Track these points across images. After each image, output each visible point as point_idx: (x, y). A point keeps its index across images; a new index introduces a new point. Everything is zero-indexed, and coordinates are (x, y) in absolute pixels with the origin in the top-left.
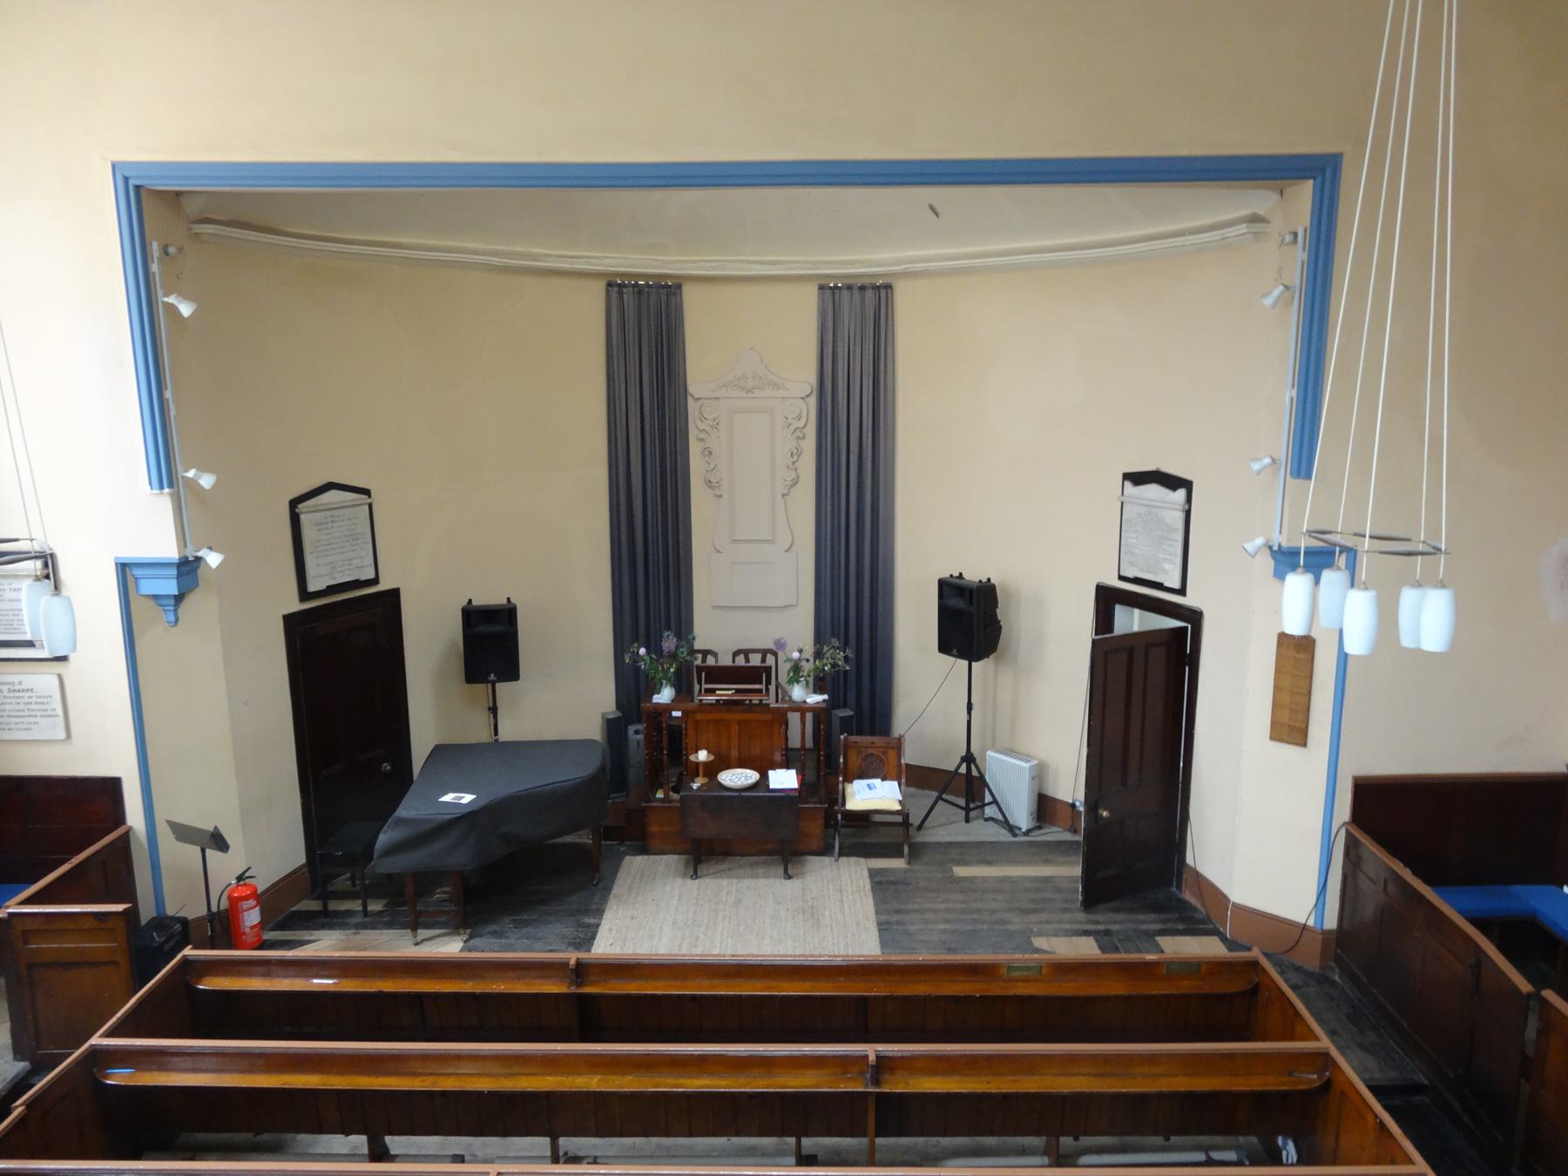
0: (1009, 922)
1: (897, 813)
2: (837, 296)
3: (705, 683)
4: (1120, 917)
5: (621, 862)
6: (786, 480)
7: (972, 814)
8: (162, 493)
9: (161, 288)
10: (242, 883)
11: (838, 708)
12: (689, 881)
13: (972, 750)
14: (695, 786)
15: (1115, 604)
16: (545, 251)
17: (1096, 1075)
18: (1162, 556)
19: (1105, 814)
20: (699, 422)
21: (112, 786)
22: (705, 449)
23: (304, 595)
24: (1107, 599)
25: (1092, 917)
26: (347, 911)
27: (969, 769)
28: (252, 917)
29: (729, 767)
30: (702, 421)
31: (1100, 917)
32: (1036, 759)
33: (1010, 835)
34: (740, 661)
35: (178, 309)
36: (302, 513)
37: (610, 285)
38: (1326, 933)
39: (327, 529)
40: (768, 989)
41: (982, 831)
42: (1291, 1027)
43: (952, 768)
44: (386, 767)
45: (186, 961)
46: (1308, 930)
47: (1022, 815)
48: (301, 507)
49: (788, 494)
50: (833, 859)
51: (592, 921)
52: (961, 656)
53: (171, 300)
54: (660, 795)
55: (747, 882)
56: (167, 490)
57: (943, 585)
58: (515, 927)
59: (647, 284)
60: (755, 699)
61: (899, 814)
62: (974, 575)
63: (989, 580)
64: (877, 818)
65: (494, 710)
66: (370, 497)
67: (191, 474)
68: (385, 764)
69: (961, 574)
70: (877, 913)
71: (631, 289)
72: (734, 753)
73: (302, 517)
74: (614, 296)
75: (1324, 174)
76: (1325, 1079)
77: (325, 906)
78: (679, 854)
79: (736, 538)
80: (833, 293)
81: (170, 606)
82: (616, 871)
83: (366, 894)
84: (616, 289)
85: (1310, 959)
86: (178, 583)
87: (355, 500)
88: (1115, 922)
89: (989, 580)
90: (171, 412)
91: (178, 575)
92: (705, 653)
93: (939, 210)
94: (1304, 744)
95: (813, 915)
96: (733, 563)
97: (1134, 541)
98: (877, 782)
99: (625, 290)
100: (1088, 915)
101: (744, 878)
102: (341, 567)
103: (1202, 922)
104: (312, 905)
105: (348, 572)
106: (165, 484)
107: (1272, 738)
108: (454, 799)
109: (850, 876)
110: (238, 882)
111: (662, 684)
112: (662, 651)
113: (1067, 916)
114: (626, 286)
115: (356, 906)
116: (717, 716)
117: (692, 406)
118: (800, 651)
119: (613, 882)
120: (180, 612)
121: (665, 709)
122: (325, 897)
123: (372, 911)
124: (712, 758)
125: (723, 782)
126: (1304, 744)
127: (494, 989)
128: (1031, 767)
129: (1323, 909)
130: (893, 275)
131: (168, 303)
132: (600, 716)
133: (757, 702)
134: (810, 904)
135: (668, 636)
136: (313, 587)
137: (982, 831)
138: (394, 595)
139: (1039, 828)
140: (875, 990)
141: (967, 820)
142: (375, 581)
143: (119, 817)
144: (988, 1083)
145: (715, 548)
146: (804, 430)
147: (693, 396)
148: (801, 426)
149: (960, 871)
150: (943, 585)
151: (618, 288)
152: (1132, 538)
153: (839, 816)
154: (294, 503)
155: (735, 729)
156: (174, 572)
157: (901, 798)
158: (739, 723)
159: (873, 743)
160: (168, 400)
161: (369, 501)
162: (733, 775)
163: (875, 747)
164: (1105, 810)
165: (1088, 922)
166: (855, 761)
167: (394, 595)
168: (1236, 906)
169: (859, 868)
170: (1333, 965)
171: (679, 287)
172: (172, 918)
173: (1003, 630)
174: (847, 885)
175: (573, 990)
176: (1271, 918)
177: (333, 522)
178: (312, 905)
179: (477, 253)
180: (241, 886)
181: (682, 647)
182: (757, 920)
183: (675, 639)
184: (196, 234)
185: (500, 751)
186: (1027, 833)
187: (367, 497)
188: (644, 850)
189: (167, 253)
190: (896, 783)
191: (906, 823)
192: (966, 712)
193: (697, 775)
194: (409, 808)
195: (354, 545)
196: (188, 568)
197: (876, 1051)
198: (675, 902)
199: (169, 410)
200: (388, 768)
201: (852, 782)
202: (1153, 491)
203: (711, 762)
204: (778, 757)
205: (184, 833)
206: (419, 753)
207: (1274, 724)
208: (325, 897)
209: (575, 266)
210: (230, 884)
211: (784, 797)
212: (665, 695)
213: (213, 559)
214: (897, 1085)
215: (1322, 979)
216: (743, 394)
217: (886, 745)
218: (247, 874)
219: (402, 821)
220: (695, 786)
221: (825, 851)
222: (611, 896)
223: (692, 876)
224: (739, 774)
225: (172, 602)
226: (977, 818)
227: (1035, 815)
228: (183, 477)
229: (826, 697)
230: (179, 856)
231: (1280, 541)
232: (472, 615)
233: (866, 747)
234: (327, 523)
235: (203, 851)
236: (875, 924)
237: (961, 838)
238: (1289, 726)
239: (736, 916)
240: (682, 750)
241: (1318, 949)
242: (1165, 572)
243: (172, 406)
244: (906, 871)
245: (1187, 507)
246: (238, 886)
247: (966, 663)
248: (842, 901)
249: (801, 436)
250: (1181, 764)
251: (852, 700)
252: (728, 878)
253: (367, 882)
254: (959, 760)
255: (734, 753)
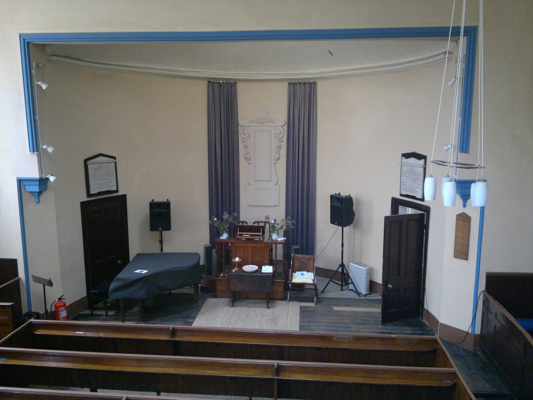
0: (351, 328)
1: (312, 284)
2: (295, 86)
3: (239, 232)
4: (396, 328)
5: (205, 300)
6: (275, 158)
7: (344, 288)
8: (34, 154)
9: (36, 79)
10: (60, 301)
11: (294, 245)
12: (230, 308)
13: (344, 262)
14: (233, 271)
15: (399, 205)
16: (184, 69)
17: (363, 377)
18: (416, 186)
19: (390, 286)
20: (242, 135)
21: (14, 262)
22: (245, 146)
23: (89, 195)
24: (396, 203)
25: (386, 327)
26: (100, 314)
27: (342, 270)
28: (63, 314)
29: (248, 264)
30: (243, 134)
31: (388, 328)
32: (369, 266)
33: (358, 296)
34: (256, 225)
35: (41, 86)
36: (89, 164)
37: (209, 82)
38: (476, 336)
39: (98, 171)
40: (245, 341)
41: (347, 294)
42: (447, 364)
43: (335, 269)
44: (119, 262)
45: (31, 323)
46: (469, 334)
47: (363, 288)
48: (89, 162)
49: (276, 163)
50: (287, 302)
51: (191, 321)
52: (339, 225)
53: (39, 83)
54: (222, 275)
55: (252, 309)
56: (36, 153)
57: (332, 197)
58: (161, 322)
59: (223, 82)
60: (257, 239)
61: (312, 285)
62: (344, 194)
63: (350, 195)
64: (307, 287)
65: (161, 242)
66: (115, 159)
67: (44, 147)
68: (119, 261)
69: (339, 193)
70: (300, 322)
71: (217, 84)
72: (250, 259)
73: (89, 166)
74: (211, 87)
75: (471, 34)
76: (454, 383)
77: (92, 312)
78: (228, 298)
79: (256, 179)
80: (294, 86)
81: (37, 196)
82: (203, 304)
83: (107, 309)
84: (211, 84)
85: (470, 346)
86: (39, 187)
87: (109, 160)
88: (394, 330)
89: (350, 195)
90: (38, 124)
91: (39, 184)
92: (243, 222)
93: (332, 53)
94: (467, 259)
95: (275, 322)
96: (255, 189)
97: (405, 180)
98: (305, 273)
99: (215, 84)
100: (383, 327)
101: (251, 307)
102: (103, 185)
103: (429, 331)
104: (88, 312)
105: (106, 187)
106: (35, 151)
107: (455, 257)
108: (140, 272)
109: (292, 308)
110: (59, 300)
111: (223, 232)
112: (223, 219)
113: (375, 326)
114: (215, 83)
115: (104, 313)
116: (244, 245)
117: (240, 129)
118: (275, 220)
119: (201, 307)
120: (40, 198)
121: (225, 243)
122: (92, 309)
123: (110, 315)
124: (241, 260)
125: (244, 269)
126: (467, 259)
127: (142, 338)
128: (367, 269)
129: (475, 326)
130: (316, 78)
131: (38, 84)
132: (203, 246)
133: (258, 239)
134: (275, 317)
135: (225, 213)
136: (92, 192)
137: (347, 294)
138: (124, 197)
139: (370, 294)
140: (285, 343)
141: (342, 290)
142: (117, 191)
143: (16, 274)
144: (321, 377)
145: (249, 183)
146: (282, 139)
147: (240, 125)
148: (281, 137)
149: (336, 308)
150: (332, 197)
151: (212, 83)
152: (405, 179)
153: (290, 285)
154: (86, 161)
155: (250, 250)
156: (38, 183)
157: (313, 279)
158: (252, 247)
159: (304, 257)
160: (37, 120)
161: (115, 161)
162: (248, 267)
163: (304, 259)
164: (391, 284)
165: (384, 329)
166: (297, 264)
167: (124, 197)
168: (441, 324)
169: (296, 305)
170: (478, 348)
171: (235, 83)
172: (34, 313)
173: (356, 215)
174: (290, 311)
175: (171, 339)
176: (462, 332)
177: (100, 168)
178: (88, 312)
179: (160, 70)
180: (60, 302)
181: (230, 218)
182: (253, 323)
183: (228, 215)
184: (51, 60)
185: (162, 256)
186: (365, 296)
187: (114, 159)
188: (215, 296)
189: (38, 66)
190: (313, 273)
191: (316, 289)
192: (341, 247)
193: (235, 267)
194: (124, 275)
195: (109, 177)
196: (43, 182)
197: (278, 363)
198: (223, 315)
199: (37, 123)
200: (120, 262)
201: (295, 272)
202: (412, 160)
203: (240, 262)
204: (266, 262)
205: (37, 279)
206: (132, 255)
207: (456, 251)
208: (92, 309)
209: (196, 75)
210: (56, 301)
211: (267, 275)
212: (225, 236)
213: (52, 179)
214: (285, 377)
215: (475, 354)
216: (260, 124)
217: (309, 258)
218: (62, 298)
219: (119, 279)
220: (233, 271)
221: (284, 299)
222: (200, 312)
223: (232, 306)
224: (251, 267)
225: (37, 194)
226: (346, 289)
227: (368, 289)
228: (42, 148)
229: (285, 238)
230: (36, 288)
231: (455, 178)
232: (153, 205)
233: (302, 259)
234: (98, 169)
235: (44, 286)
236: (299, 326)
237: (338, 297)
238: (461, 251)
239: (246, 321)
240: (230, 258)
241: (473, 342)
242: (416, 192)
243: (38, 122)
244: (314, 307)
245: (424, 166)
246: (59, 302)
247: (340, 228)
248: (287, 317)
249: (281, 141)
250: (423, 266)
251: (299, 242)
252: (245, 307)
253: (108, 305)
254: (338, 266)
255: (250, 259)
